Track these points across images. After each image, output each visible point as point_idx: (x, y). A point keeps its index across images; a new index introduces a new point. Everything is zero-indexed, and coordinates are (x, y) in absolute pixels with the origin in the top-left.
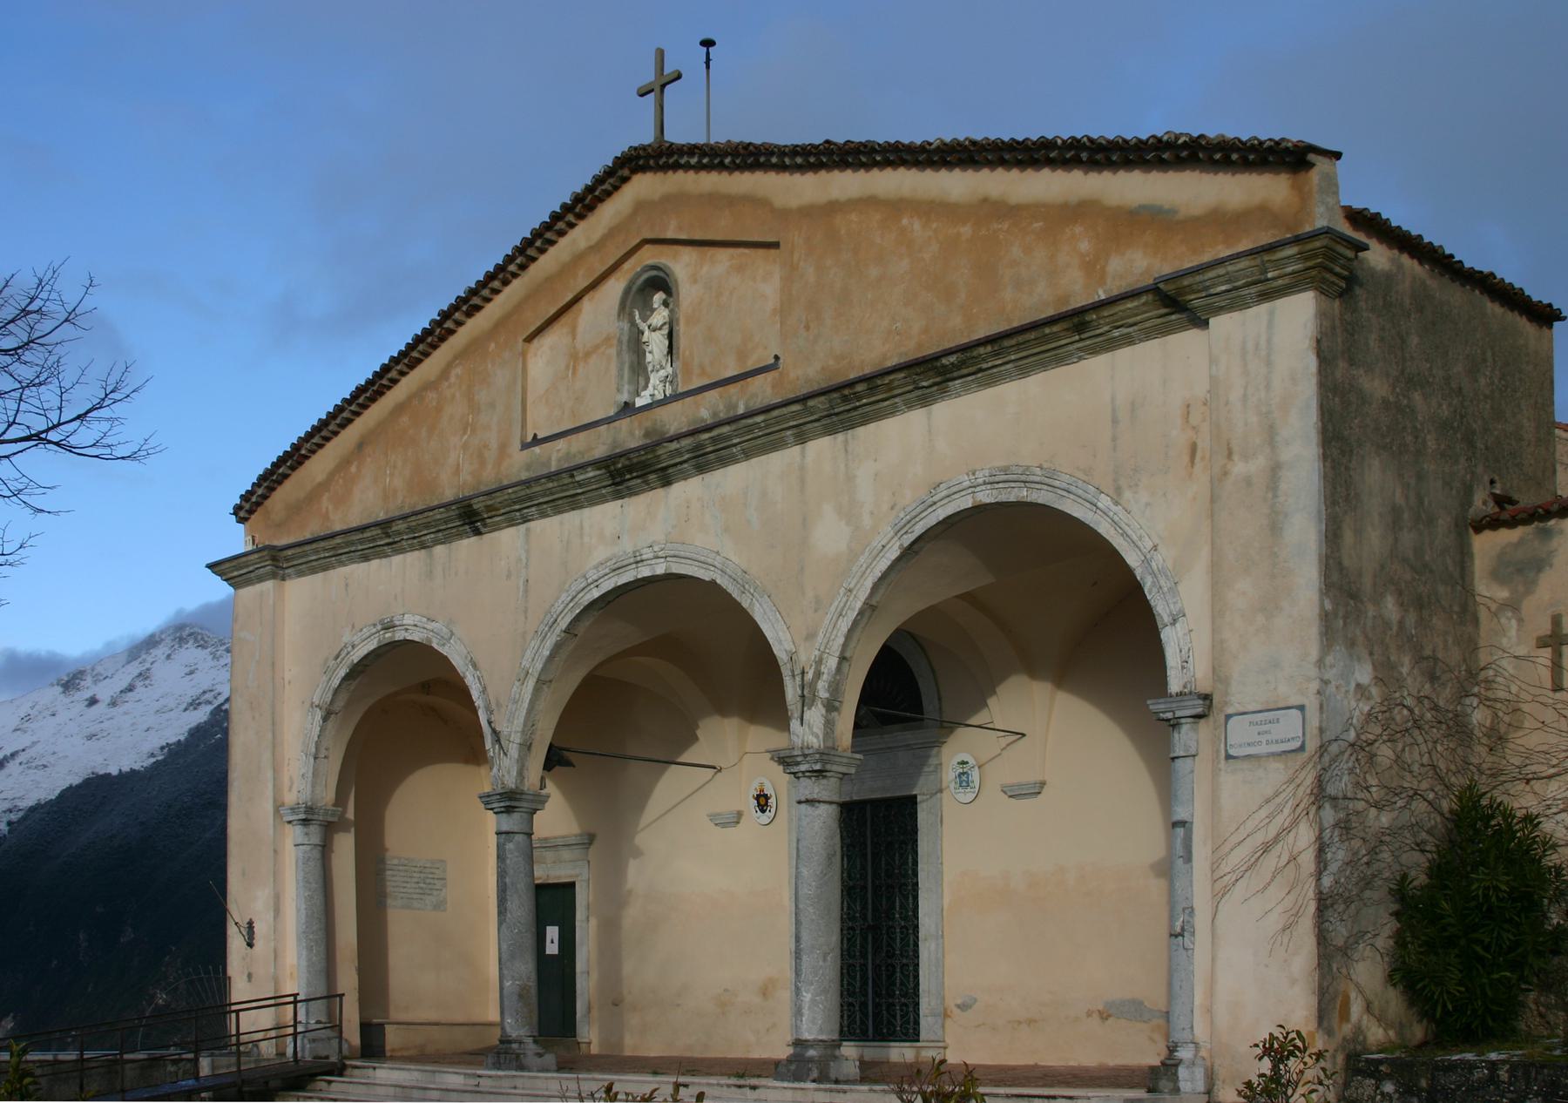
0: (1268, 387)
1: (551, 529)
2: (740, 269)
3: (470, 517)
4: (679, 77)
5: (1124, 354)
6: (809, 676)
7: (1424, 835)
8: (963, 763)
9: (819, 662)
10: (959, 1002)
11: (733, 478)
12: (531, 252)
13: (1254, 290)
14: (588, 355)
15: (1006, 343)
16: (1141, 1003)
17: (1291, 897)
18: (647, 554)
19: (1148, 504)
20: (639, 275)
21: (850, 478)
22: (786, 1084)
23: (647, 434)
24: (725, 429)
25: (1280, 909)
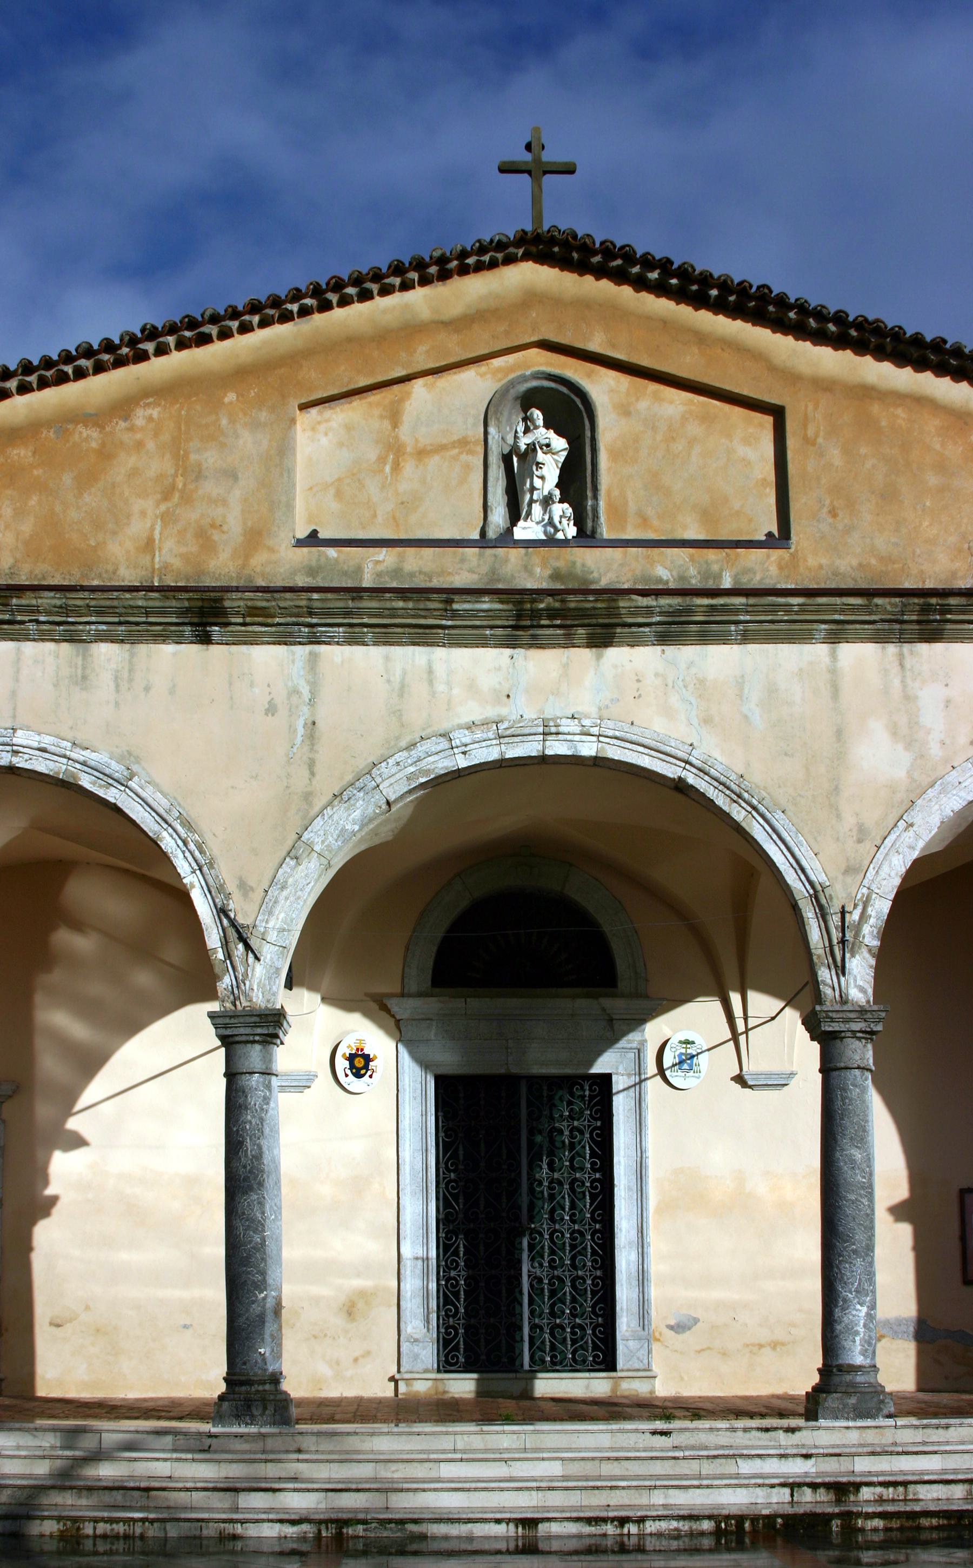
1: (362, 669)
2: (706, 418)
3: (204, 613)
4: (572, 172)
7: (248, 1168)
8: (687, 1042)
9: (866, 903)
10: (672, 1322)
11: (719, 660)
12: (333, 298)
14: (422, 454)
20: (524, 379)
21: (909, 698)
23: (556, 575)
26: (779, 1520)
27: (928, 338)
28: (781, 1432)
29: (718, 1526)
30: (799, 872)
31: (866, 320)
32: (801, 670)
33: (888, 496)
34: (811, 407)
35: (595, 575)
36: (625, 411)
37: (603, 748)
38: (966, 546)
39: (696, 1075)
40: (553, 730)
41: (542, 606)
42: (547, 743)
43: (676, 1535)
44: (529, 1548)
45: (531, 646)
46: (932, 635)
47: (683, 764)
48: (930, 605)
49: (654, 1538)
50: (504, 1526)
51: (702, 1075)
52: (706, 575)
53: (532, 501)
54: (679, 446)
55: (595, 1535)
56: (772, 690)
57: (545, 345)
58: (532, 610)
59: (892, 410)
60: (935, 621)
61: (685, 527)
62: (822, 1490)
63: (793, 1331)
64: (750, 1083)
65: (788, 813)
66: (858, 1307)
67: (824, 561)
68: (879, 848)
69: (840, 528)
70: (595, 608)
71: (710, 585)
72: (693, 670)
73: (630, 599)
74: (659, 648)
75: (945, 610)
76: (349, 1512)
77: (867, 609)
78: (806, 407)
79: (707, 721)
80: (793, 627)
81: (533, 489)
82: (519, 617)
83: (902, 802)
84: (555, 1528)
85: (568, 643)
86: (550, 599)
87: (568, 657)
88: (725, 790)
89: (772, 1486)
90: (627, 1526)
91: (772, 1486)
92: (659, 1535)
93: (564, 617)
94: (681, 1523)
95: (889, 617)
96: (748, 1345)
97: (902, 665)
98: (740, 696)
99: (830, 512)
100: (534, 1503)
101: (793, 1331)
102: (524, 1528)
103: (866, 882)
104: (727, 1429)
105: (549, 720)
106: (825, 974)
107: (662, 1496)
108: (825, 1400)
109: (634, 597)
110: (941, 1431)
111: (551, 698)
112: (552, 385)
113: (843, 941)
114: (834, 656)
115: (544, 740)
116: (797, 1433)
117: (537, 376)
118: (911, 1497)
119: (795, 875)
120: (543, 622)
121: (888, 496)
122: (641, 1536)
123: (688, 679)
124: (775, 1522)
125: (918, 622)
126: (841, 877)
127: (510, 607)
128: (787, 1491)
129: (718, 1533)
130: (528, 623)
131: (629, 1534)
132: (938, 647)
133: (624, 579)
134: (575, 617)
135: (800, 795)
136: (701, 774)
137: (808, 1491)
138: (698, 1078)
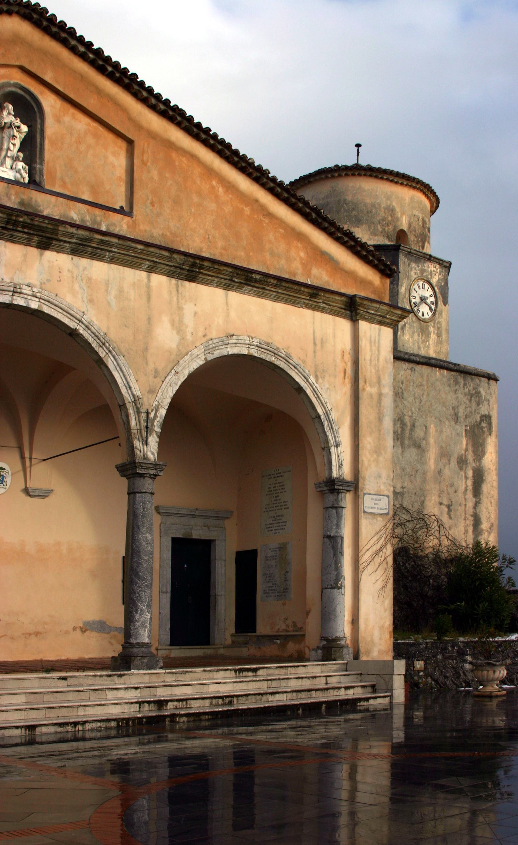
0: (378, 359)
2: (96, 136)
5: (318, 315)
6: (152, 415)
11: (99, 270)
13: (379, 318)
15: (284, 284)
16: (105, 623)
17: (385, 574)
18: (26, 290)
19: (328, 388)
20: (9, 85)
21: (180, 308)
22: (141, 672)
24: (115, 240)
25: (381, 579)
26: (144, 720)
27: (204, 126)
28: (116, 677)
29: (118, 724)
30: (128, 389)
31: (178, 107)
32: (134, 283)
33: (177, 202)
34: (146, 145)
35: (41, 208)
36: (58, 120)
37: (41, 305)
38: (207, 236)
39: (4, 487)
40: (19, 290)
41: (21, 220)
42: (14, 297)
43: (99, 729)
44: (31, 742)
45: (8, 240)
46: (192, 278)
47: (78, 322)
48: (196, 263)
49: (90, 732)
50: (19, 730)
51: (7, 487)
52: (94, 222)
53: (6, 156)
54: (83, 148)
55: (63, 732)
56: (121, 291)
57: (23, 69)
58: (15, 221)
59: (181, 157)
60: (196, 271)
61: (83, 193)
62: (152, 705)
63: (46, 627)
64: (31, 494)
65: (126, 357)
66: (147, 614)
67: (147, 228)
68: (163, 382)
69: (155, 213)
70: (47, 227)
71: (96, 227)
72: (86, 272)
73: (65, 227)
74: (70, 256)
75: (201, 267)
76: (115, 715)
77: (170, 259)
78: (144, 145)
79: (91, 301)
80: (134, 260)
81: (8, 149)
82: (8, 223)
83: (174, 360)
84: (44, 730)
85: (28, 243)
86: (26, 217)
87: (26, 251)
88: (97, 340)
89: (132, 703)
90: (77, 726)
91: (132, 703)
92: (92, 730)
93: (30, 229)
94: (102, 724)
95: (177, 265)
96: (24, 634)
97: (177, 290)
98: (107, 291)
99: (151, 203)
100: (23, 717)
101: (46, 627)
102: (29, 730)
103: (157, 399)
104: (93, 676)
105: (17, 284)
106: (137, 444)
107: (83, 711)
108: (134, 660)
109: (67, 226)
110: (183, 675)
111: (18, 272)
112: (22, 93)
113: (147, 427)
114: (149, 278)
115: (13, 295)
116: (123, 677)
117: (16, 85)
118: (188, 706)
119: (126, 390)
120: (19, 229)
121: (177, 202)
122: (84, 731)
123: (83, 276)
124: (143, 721)
125: (188, 270)
126: (146, 394)
127: (5, 216)
128: (138, 705)
129: (118, 727)
130: (11, 227)
131: (78, 731)
132: (193, 285)
133: (55, 214)
134: (35, 230)
135: (131, 349)
136: (87, 329)
137: (146, 705)
138: (5, 488)
